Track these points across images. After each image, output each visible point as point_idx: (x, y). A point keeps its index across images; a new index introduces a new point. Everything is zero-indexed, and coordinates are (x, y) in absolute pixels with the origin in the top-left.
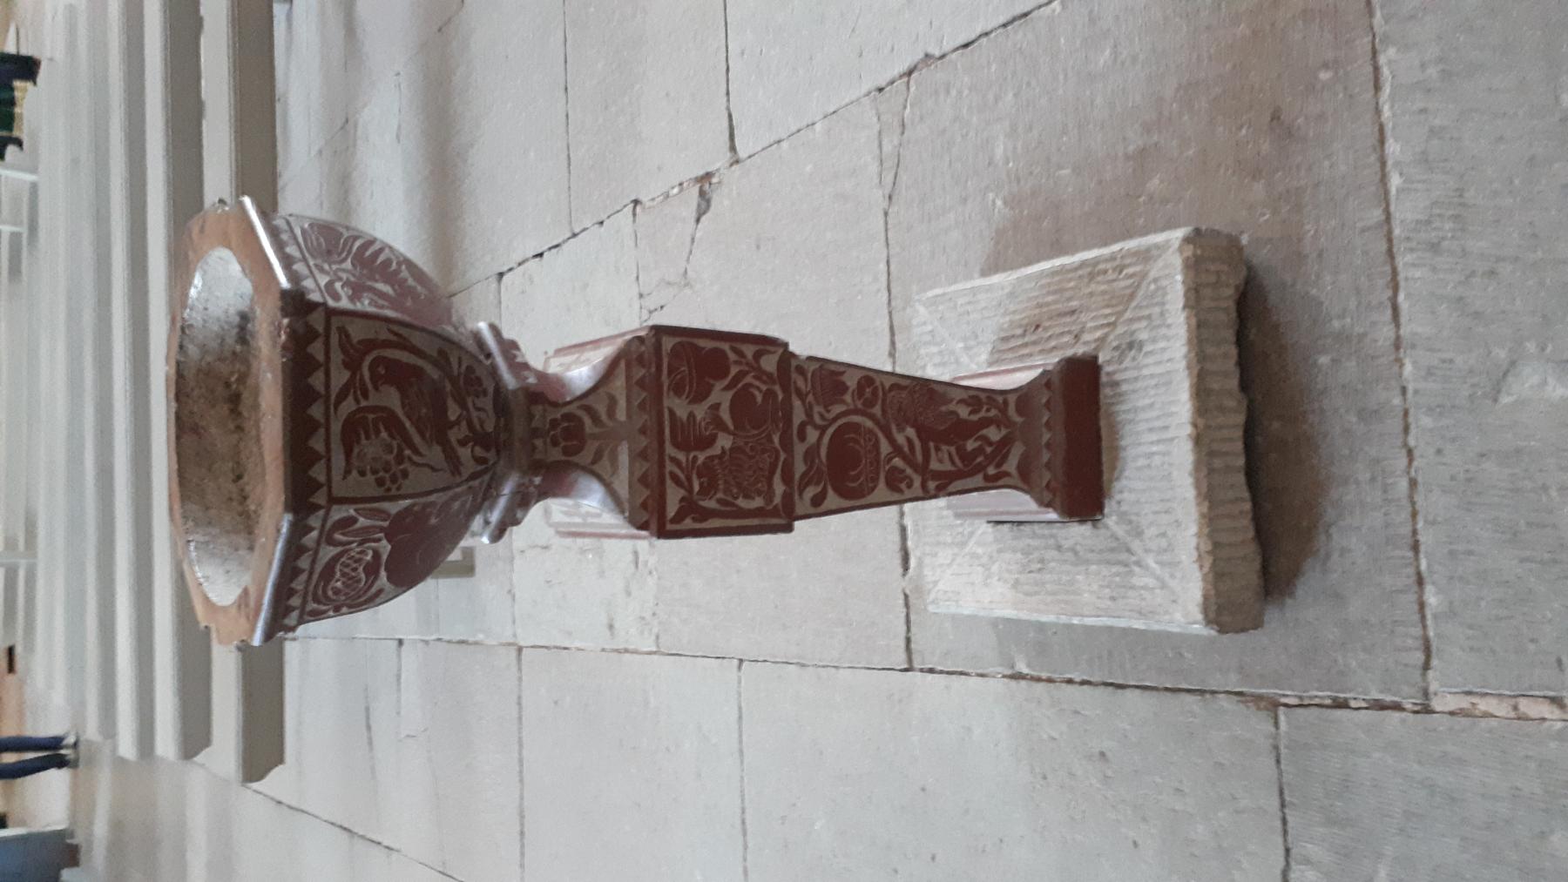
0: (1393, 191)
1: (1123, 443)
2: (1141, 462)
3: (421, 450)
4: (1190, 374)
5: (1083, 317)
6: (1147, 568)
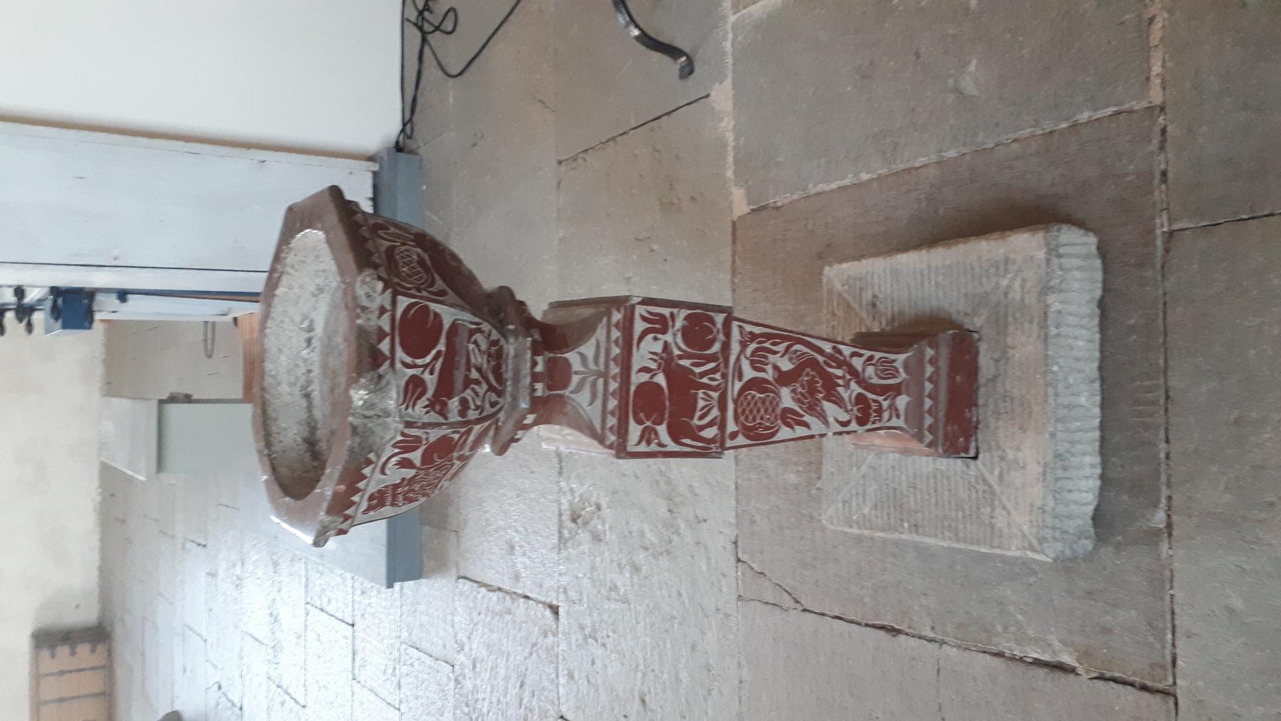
2: (941, 294)
6: (1009, 287)
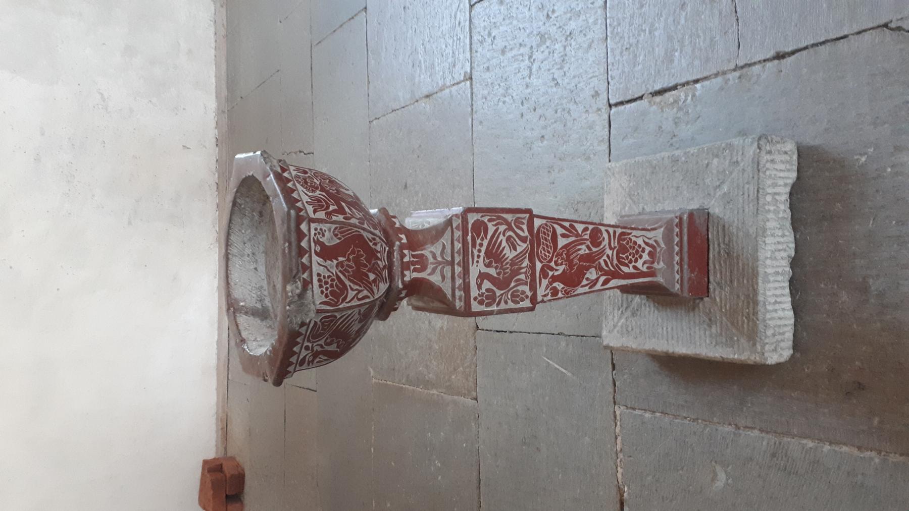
0: (804, 441)
1: (668, 310)
3: (322, 305)
4: (694, 355)
5: (727, 289)
6: (620, 318)
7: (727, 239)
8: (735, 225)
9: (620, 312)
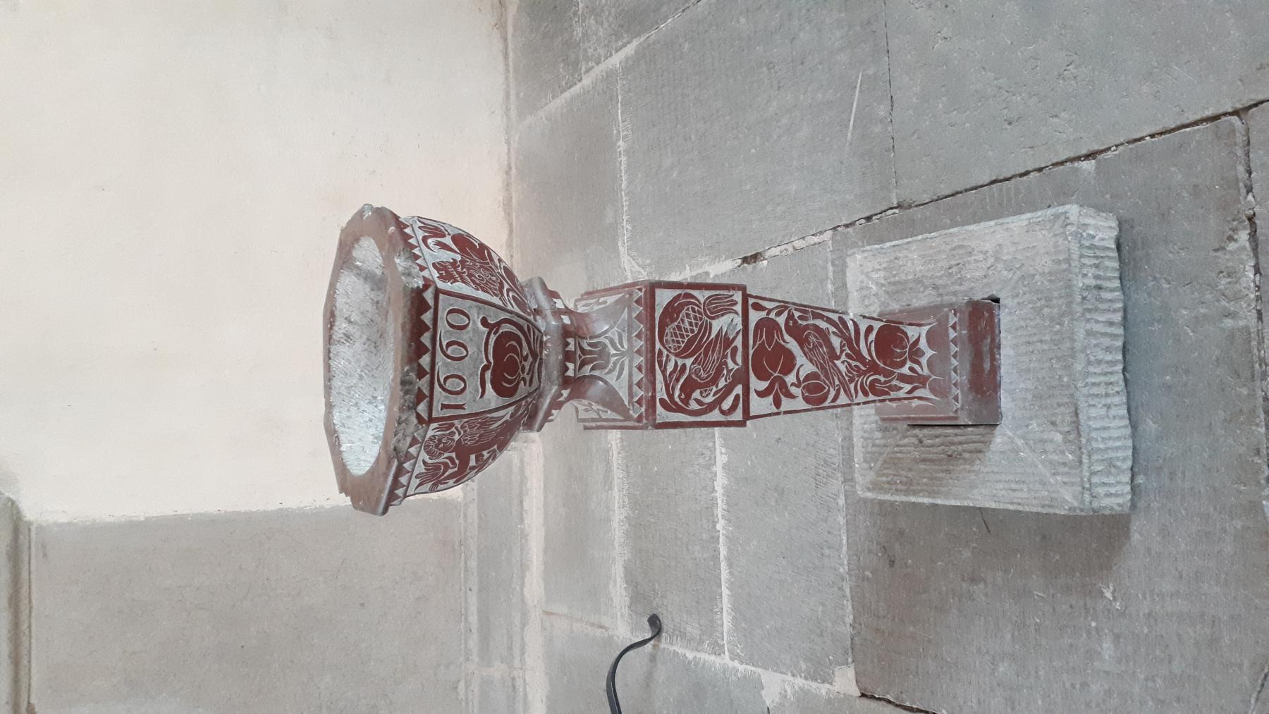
0: (843, 498)
7: (967, 455)
8: (982, 469)
9: (883, 282)
